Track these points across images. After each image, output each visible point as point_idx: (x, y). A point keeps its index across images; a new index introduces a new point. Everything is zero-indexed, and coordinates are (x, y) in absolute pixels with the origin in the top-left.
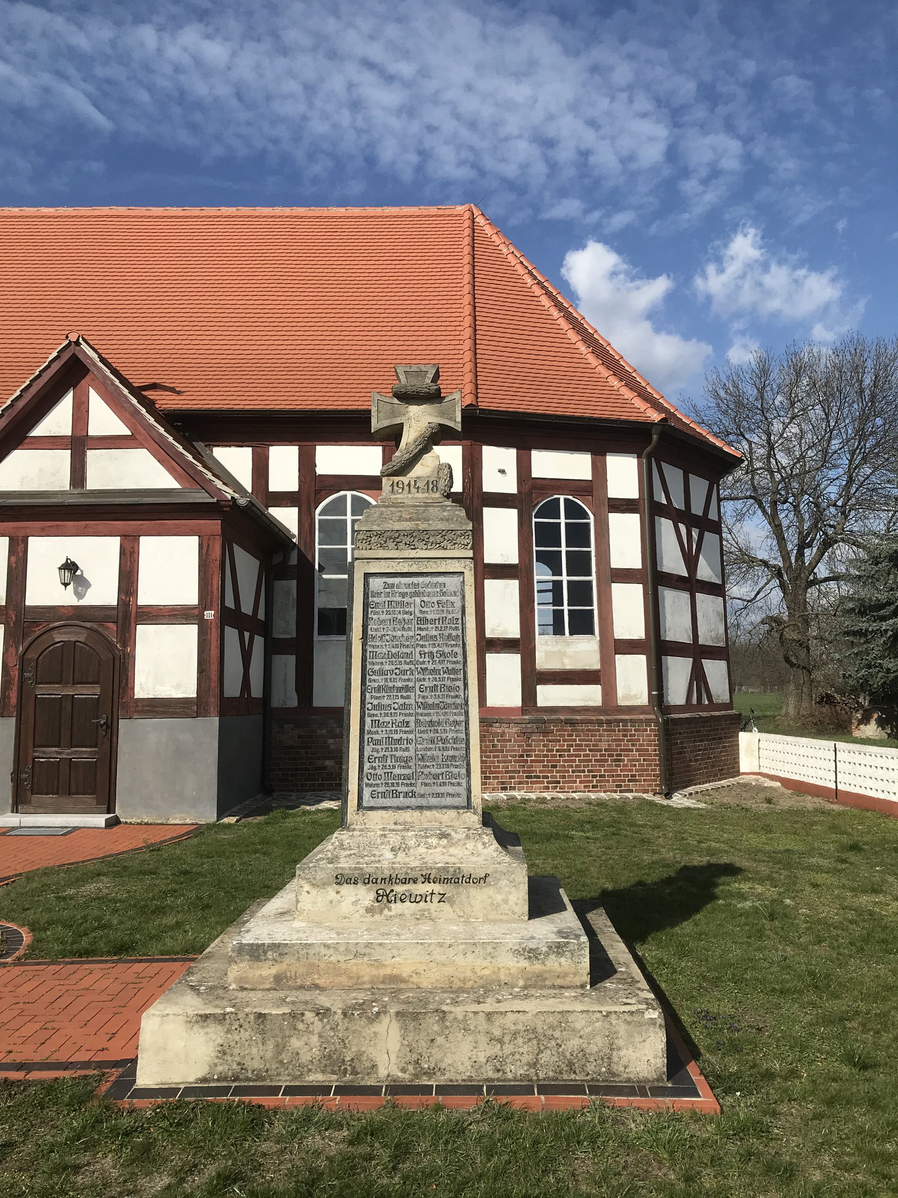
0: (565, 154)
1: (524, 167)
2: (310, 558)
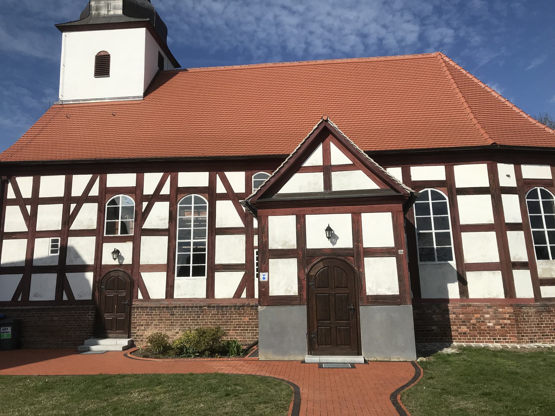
0: (372, 40)
1: (353, 47)
2: (412, 222)
